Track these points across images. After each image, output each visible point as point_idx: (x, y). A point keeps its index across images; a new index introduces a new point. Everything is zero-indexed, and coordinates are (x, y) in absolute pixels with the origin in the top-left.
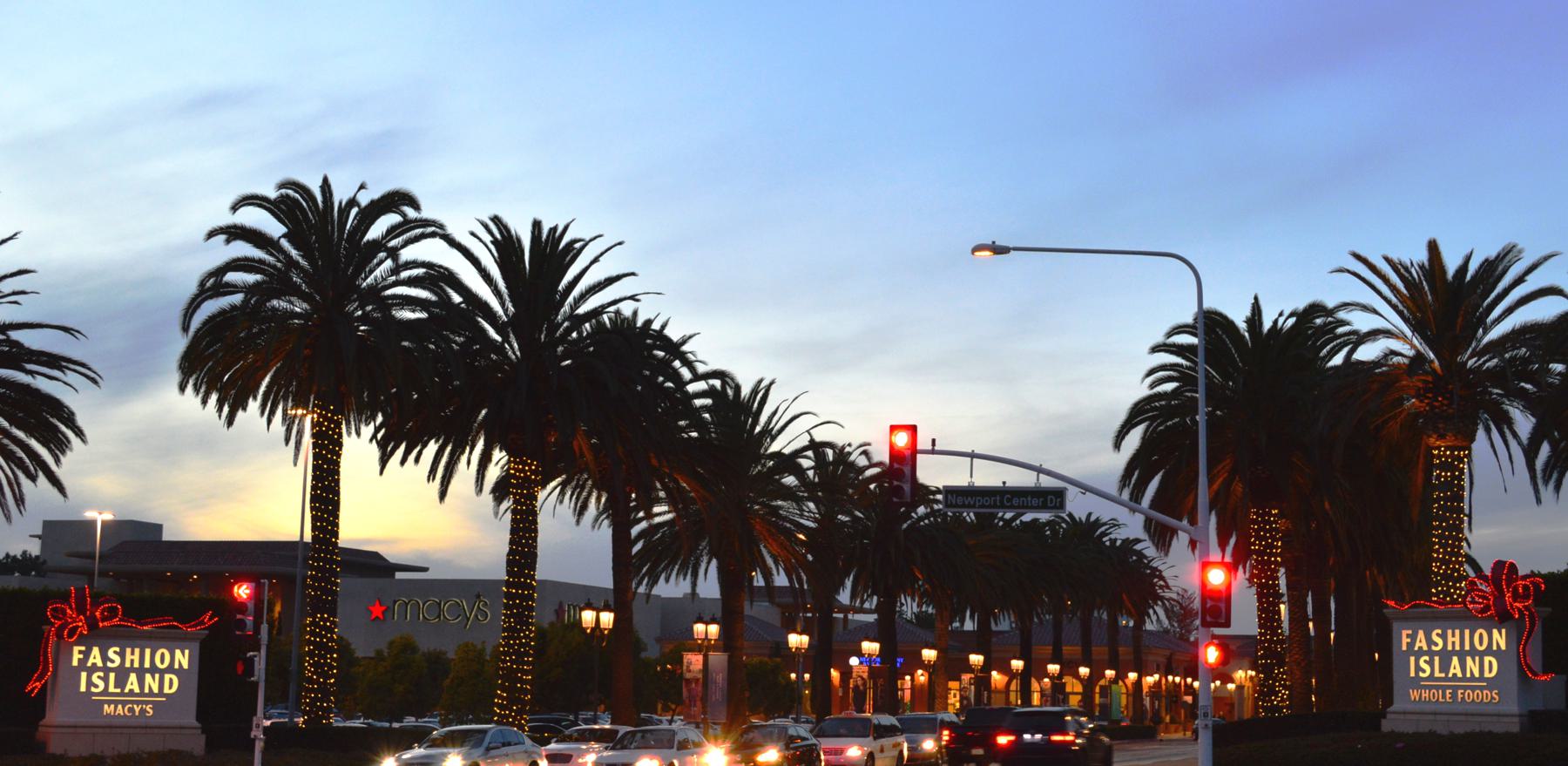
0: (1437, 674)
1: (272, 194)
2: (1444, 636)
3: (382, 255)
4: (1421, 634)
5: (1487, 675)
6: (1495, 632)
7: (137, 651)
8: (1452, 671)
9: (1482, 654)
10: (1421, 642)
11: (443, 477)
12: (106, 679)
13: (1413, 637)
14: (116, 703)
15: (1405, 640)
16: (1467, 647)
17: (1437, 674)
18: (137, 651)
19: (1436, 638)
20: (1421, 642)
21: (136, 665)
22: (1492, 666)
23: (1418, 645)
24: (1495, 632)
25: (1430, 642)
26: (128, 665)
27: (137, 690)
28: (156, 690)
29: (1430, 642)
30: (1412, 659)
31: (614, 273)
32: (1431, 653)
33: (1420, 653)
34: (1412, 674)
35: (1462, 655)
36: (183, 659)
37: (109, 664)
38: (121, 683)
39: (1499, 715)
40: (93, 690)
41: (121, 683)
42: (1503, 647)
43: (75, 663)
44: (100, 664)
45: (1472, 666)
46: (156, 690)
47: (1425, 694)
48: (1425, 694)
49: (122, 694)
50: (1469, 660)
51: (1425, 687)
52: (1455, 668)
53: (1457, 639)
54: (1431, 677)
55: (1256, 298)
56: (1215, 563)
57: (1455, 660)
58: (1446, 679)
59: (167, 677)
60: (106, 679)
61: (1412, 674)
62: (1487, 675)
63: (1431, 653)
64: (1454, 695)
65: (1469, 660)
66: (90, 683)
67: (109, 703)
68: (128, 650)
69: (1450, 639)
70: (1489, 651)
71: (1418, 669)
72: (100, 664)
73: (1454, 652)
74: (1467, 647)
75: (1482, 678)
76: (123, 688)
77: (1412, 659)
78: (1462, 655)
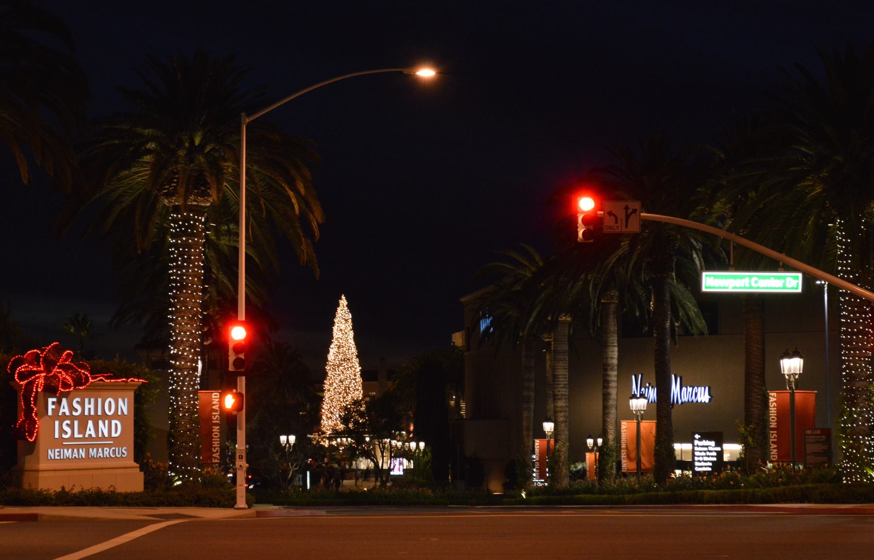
0: (76, 435)
2: (82, 404)
3: (697, 469)
5: (114, 435)
6: (120, 400)
7: (92, 400)
8: (88, 432)
9: (110, 418)
14: (73, 447)
15: (51, 407)
16: (100, 413)
17: (76, 435)
18: (92, 400)
19: (76, 405)
21: (92, 413)
22: (117, 429)
23: (62, 410)
24: (120, 400)
25: (72, 408)
26: (86, 413)
28: (106, 435)
29: (72, 408)
30: (57, 423)
32: (72, 418)
34: (57, 436)
36: (124, 406)
37: (74, 413)
39: (79, 469)
40: (64, 436)
41: (83, 428)
42: (126, 413)
45: (103, 427)
46: (106, 435)
47: (68, 453)
48: (68, 453)
49: (84, 439)
50: (100, 422)
51: (68, 447)
52: (90, 431)
53: (92, 406)
54: (72, 438)
56: (643, 417)
57: (90, 424)
58: (84, 439)
59: (114, 422)
60: (71, 426)
61: (57, 436)
62: (114, 435)
64: (87, 453)
68: (87, 400)
69: (87, 406)
70: (115, 416)
72: (68, 414)
73: (90, 417)
74: (100, 413)
75: (110, 437)
76: (84, 433)
77: (57, 423)
78: (96, 419)
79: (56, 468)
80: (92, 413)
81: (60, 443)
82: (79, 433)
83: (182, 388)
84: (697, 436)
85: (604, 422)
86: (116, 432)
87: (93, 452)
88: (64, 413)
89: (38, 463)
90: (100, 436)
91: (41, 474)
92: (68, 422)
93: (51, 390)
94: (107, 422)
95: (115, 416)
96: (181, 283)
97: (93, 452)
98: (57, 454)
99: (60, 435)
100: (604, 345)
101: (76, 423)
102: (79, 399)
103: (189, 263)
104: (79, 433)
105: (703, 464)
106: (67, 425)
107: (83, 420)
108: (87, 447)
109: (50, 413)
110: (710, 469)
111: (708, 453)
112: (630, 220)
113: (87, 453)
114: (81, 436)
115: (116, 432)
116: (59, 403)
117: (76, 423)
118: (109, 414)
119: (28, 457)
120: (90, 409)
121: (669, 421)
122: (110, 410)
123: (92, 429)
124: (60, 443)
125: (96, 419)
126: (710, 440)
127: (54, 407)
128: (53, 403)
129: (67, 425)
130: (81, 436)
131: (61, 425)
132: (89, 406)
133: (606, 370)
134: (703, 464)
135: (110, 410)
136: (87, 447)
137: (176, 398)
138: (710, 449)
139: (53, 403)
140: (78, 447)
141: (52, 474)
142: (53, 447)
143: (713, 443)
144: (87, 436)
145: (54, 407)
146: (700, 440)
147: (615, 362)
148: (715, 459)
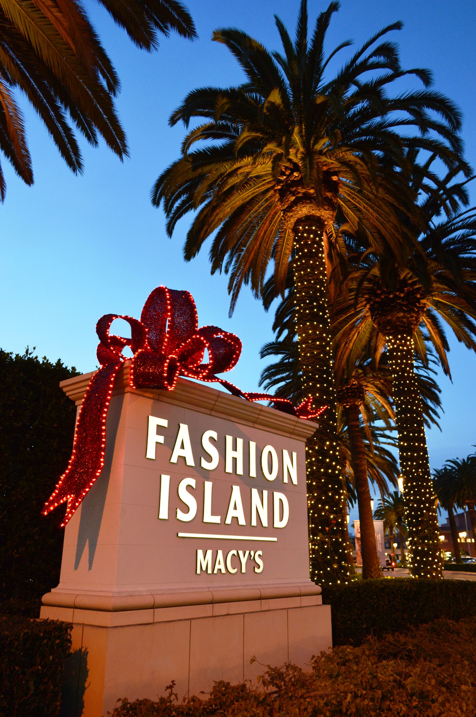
0: (209, 518)
1: (439, 407)
2: (220, 445)
4: (184, 430)
5: (278, 524)
7: (240, 442)
8: (231, 513)
10: (183, 450)
13: (170, 435)
15: (154, 439)
16: (253, 473)
17: (209, 518)
18: (209, 553)
20: (183, 450)
21: (240, 471)
23: (177, 452)
25: (199, 452)
26: (229, 469)
27: (242, 521)
28: (265, 523)
29: (199, 452)
30: (166, 480)
31: (441, 427)
32: (202, 474)
33: (179, 470)
34: (164, 514)
36: (292, 466)
40: (181, 516)
42: (295, 482)
43: (151, 454)
44: (190, 462)
46: (265, 523)
50: (255, 492)
53: (239, 455)
55: (276, 17)
59: (278, 496)
60: (198, 492)
61: (164, 514)
62: (278, 524)
63: (202, 474)
65: (255, 492)
66: (176, 503)
67: (206, 545)
68: (229, 439)
69: (230, 454)
70: (279, 485)
71: (176, 503)
72: (190, 462)
77: (166, 480)
80: (240, 471)
82: (214, 513)
86: (281, 519)
88: (182, 459)
90: (254, 523)
92: (192, 482)
94: (265, 493)
101: (208, 486)
102: (214, 434)
104: (214, 513)
106: (189, 488)
107: (223, 481)
112: (187, 689)
114: (217, 519)
115: (281, 519)
117: (208, 486)
118: (271, 477)
120: (235, 460)
122: (271, 472)
125: (248, 483)
127: (161, 439)
130: (217, 519)
135: (271, 472)
144: (228, 521)
145: (161, 439)
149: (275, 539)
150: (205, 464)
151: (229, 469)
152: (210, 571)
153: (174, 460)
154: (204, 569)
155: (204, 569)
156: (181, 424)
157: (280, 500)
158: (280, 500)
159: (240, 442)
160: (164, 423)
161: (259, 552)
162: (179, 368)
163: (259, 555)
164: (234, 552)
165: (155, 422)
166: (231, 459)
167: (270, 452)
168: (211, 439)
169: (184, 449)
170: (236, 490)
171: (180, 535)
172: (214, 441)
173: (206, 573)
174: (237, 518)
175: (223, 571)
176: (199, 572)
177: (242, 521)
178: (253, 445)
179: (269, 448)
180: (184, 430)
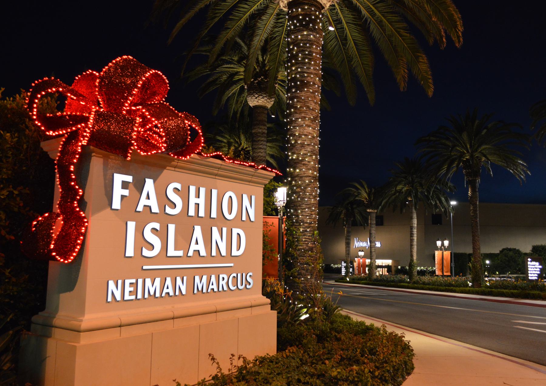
0: (172, 252)
5: (235, 253)
7: (203, 191)
8: (193, 247)
9: (231, 224)
11: (512, 293)
12: (163, 234)
14: (163, 274)
15: (118, 192)
16: (214, 215)
17: (172, 252)
21: (202, 213)
23: (143, 201)
25: (164, 201)
26: (192, 212)
29: (164, 201)
30: (131, 226)
32: (164, 218)
34: (130, 252)
35: (208, 225)
38: (184, 239)
40: (146, 253)
41: (184, 239)
42: (253, 219)
47: (153, 286)
48: (153, 286)
50: (215, 230)
51: (153, 274)
53: (202, 201)
57: (198, 232)
59: (235, 231)
60: (163, 234)
61: (130, 252)
62: (235, 253)
63: (164, 218)
64: (192, 284)
66: (142, 242)
68: (193, 189)
69: (193, 200)
70: (239, 221)
71: (142, 242)
72: (155, 209)
77: (131, 226)
78: (208, 225)
79: (125, 320)
80: (202, 213)
81: (138, 267)
83: (303, 199)
84: (529, 260)
85: (411, 251)
86: (239, 248)
87: (200, 283)
89: (83, 313)
91: (85, 340)
93: (114, 145)
95: (239, 221)
96: (302, 82)
97: (200, 283)
98: (128, 289)
99: (138, 249)
100: (411, 218)
101: (172, 228)
103: (310, 60)
105: (533, 275)
106: (154, 230)
107: (186, 223)
108: (191, 275)
109: (116, 204)
110: (536, 278)
111: (535, 269)
113: (192, 284)
114: (180, 253)
115: (239, 248)
116: (139, 186)
119: (65, 298)
120: (197, 205)
121: (371, 253)
122: (230, 213)
123: (201, 241)
124: (138, 267)
126: (536, 262)
127: (126, 192)
128: (125, 185)
129: (154, 230)
130: (133, 297)
131: (140, 232)
132: (197, 200)
133: (412, 229)
134: (533, 275)
135: (230, 213)
136: (191, 275)
137: (296, 210)
138: (536, 266)
139: (125, 185)
140: (174, 273)
141: (114, 334)
142: (119, 277)
143: (537, 264)
144: (191, 253)
146: (531, 261)
147: (416, 225)
148: (539, 272)
149: (232, 265)
150: (169, 210)
151: (192, 212)
152: (158, 295)
153: (140, 208)
154: (200, 289)
155: (200, 289)
156: (146, 179)
157: (238, 234)
158: (238, 234)
159: (203, 191)
160: (129, 179)
161: (250, 274)
162: (234, 144)
163: (250, 276)
164: (235, 275)
165: (119, 178)
166: (194, 205)
167: (231, 197)
168: (176, 190)
169: (149, 199)
170: (198, 230)
171: (145, 267)
172: (177, 191)
173: (237, 290)
174: (199, 251)
175: (216, 290)
176: (196, 291)
177: (203, 253)
178: (215, 192)
179: (229, 194)
180: (149, 184)
